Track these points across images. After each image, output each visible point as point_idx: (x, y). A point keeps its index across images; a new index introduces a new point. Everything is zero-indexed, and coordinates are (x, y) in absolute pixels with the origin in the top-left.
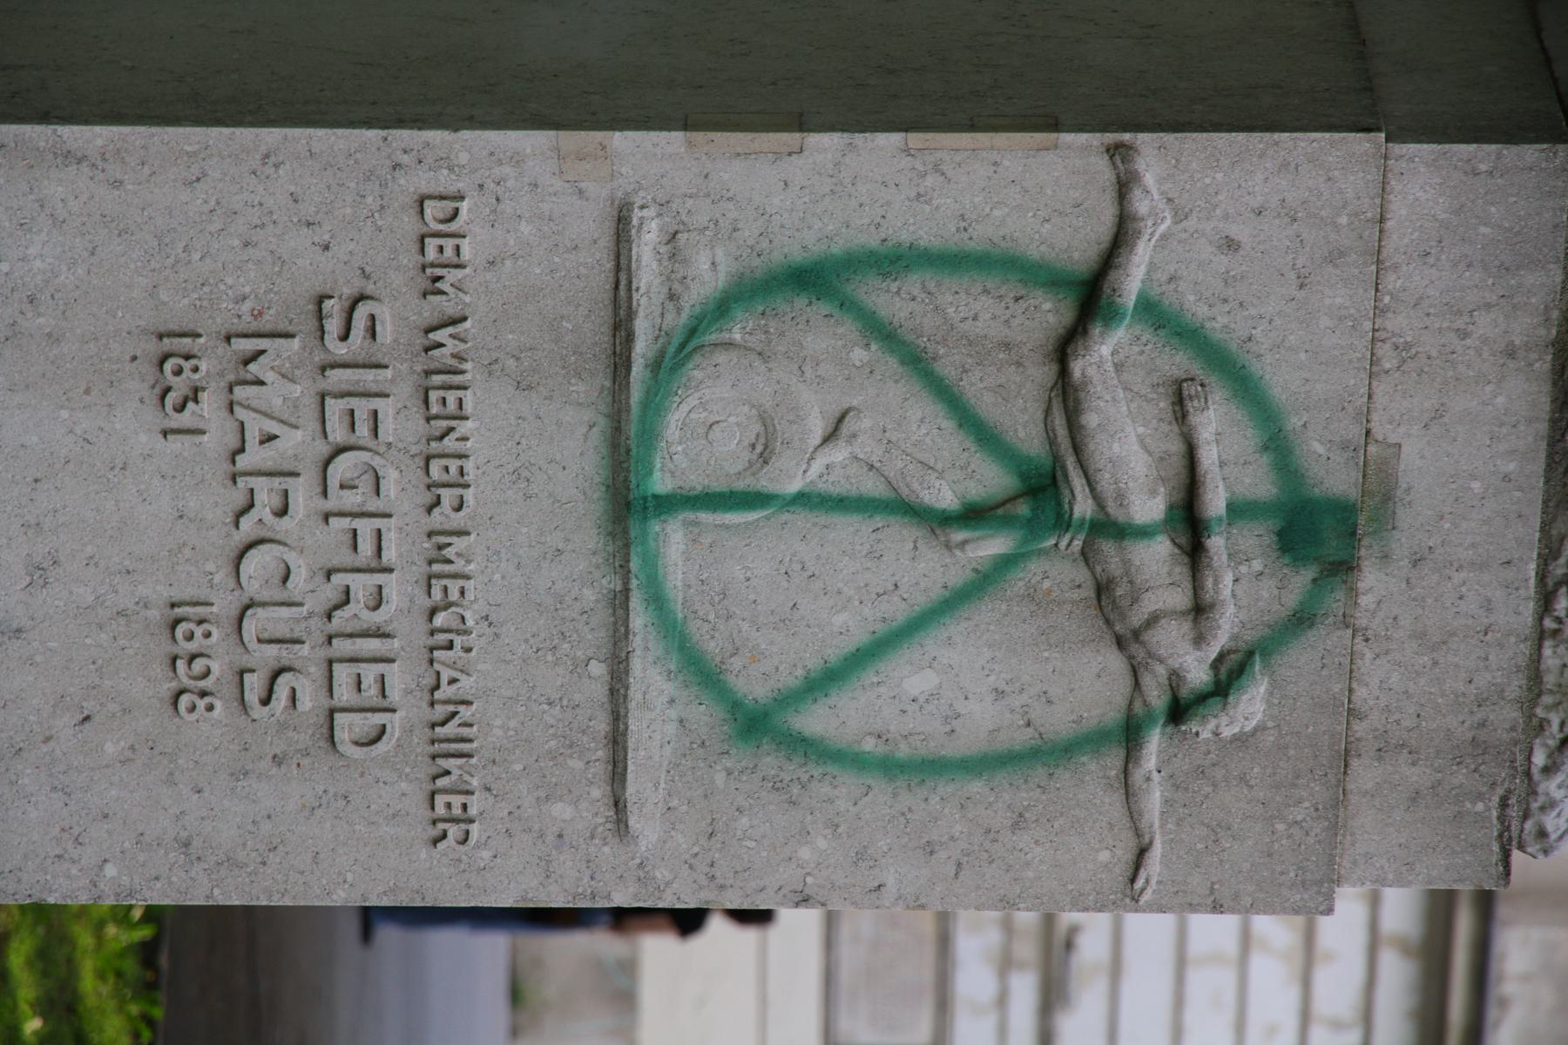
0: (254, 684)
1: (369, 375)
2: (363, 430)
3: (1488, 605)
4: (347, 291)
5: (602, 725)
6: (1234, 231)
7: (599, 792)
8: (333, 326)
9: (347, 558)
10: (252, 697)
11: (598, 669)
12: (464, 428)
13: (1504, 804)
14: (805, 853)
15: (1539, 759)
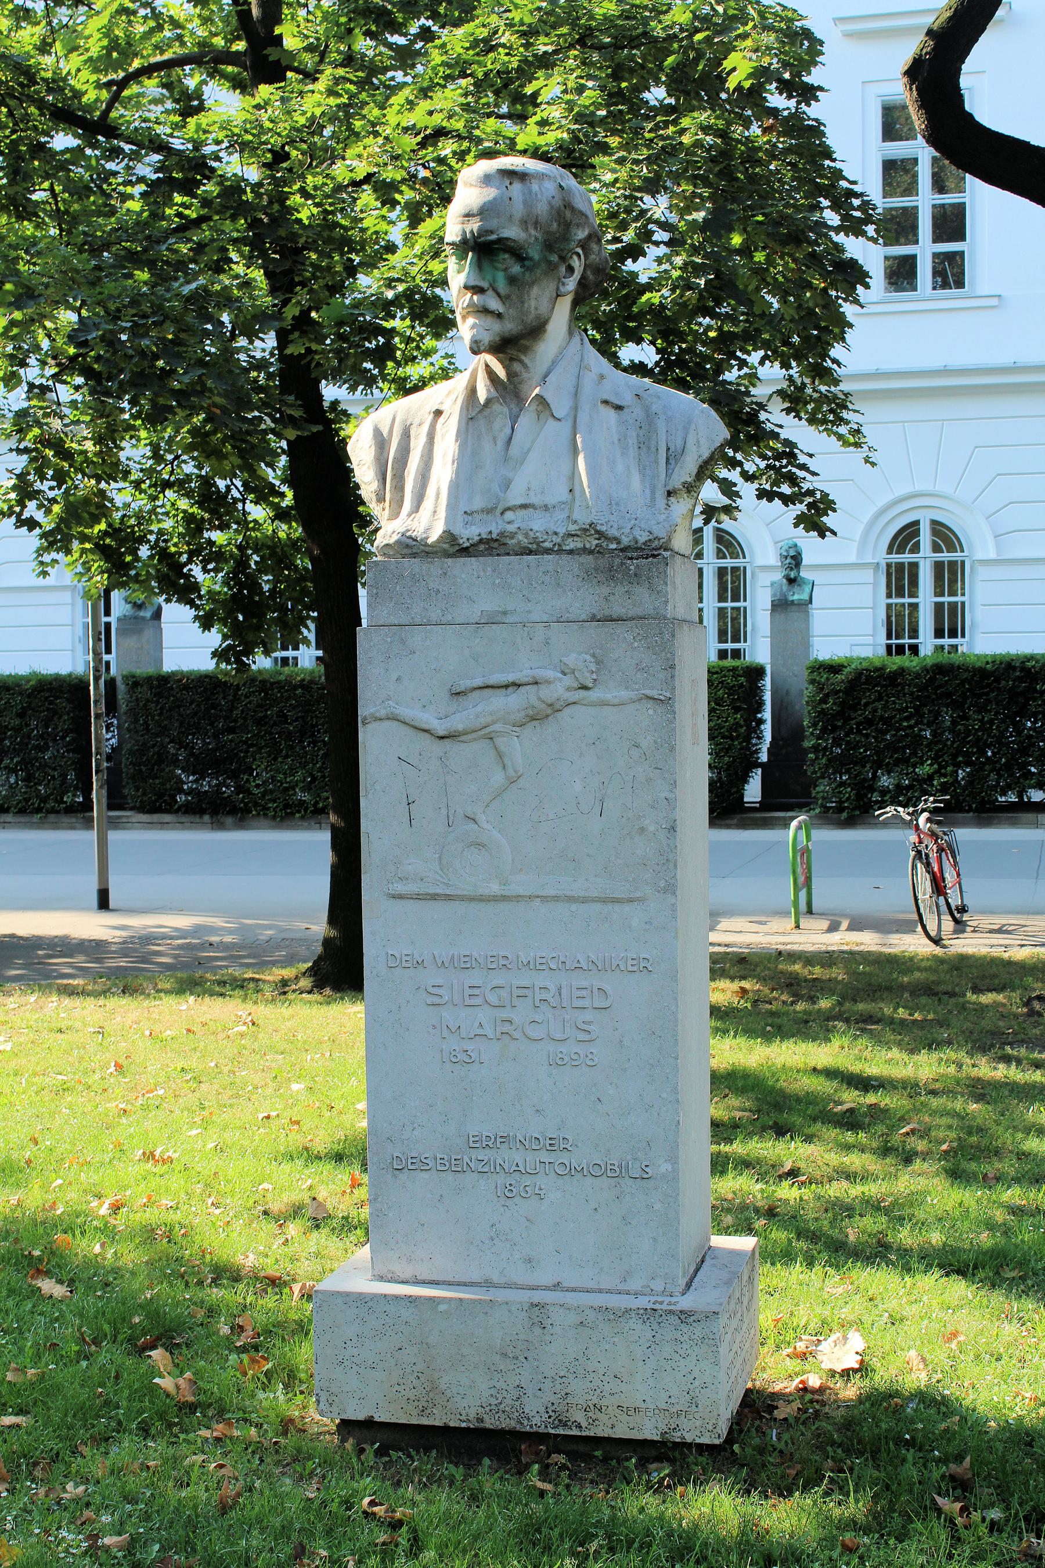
0: (582, 1036)
1: (455, 988)
2: (476, 991)
3: (546, 573)
4: (424, 994)
5: (597, 906)
6: (394, 676)
7: (627, 908)
8: (437, 1000)
9: (529, 1000)
10: (587, 1037)
11: (574, 907)
12: (475, 954)
13: (631, 559)
14: (652, 828)
15: (614, 546)
